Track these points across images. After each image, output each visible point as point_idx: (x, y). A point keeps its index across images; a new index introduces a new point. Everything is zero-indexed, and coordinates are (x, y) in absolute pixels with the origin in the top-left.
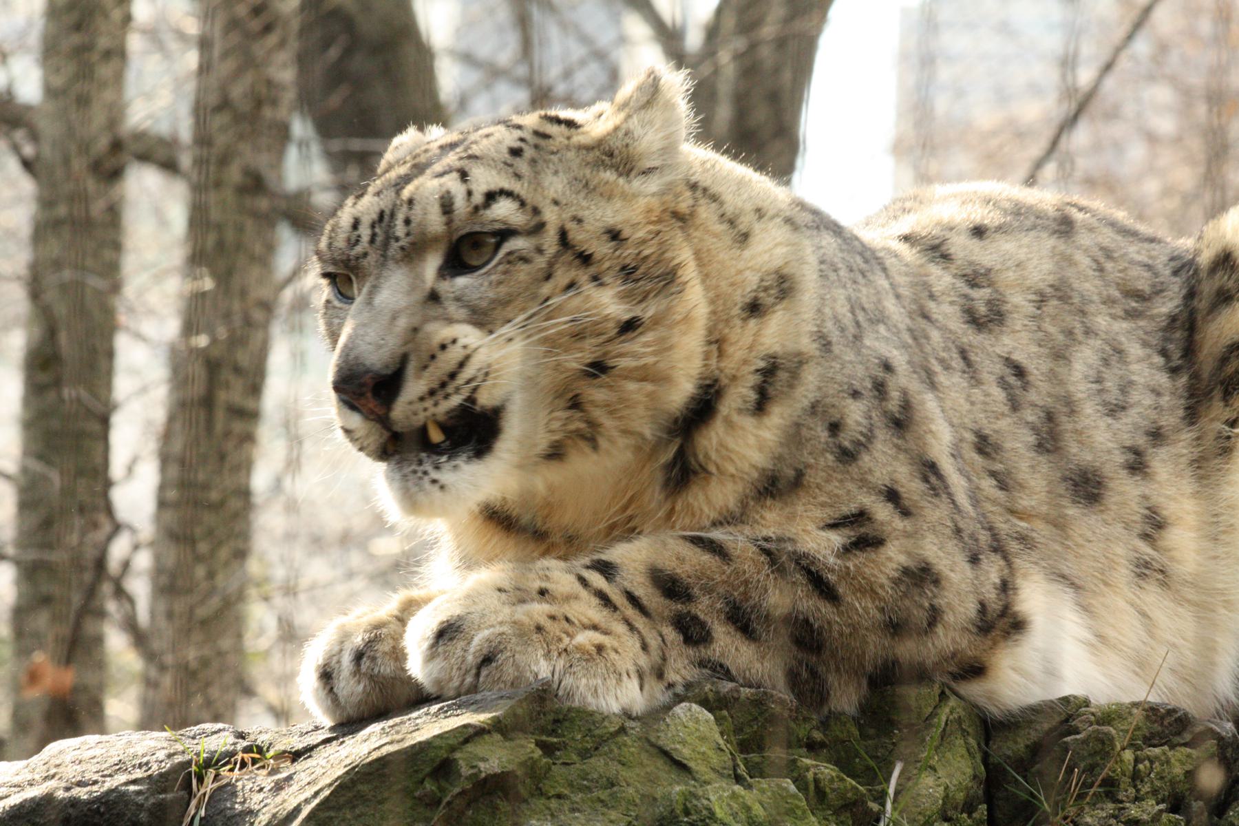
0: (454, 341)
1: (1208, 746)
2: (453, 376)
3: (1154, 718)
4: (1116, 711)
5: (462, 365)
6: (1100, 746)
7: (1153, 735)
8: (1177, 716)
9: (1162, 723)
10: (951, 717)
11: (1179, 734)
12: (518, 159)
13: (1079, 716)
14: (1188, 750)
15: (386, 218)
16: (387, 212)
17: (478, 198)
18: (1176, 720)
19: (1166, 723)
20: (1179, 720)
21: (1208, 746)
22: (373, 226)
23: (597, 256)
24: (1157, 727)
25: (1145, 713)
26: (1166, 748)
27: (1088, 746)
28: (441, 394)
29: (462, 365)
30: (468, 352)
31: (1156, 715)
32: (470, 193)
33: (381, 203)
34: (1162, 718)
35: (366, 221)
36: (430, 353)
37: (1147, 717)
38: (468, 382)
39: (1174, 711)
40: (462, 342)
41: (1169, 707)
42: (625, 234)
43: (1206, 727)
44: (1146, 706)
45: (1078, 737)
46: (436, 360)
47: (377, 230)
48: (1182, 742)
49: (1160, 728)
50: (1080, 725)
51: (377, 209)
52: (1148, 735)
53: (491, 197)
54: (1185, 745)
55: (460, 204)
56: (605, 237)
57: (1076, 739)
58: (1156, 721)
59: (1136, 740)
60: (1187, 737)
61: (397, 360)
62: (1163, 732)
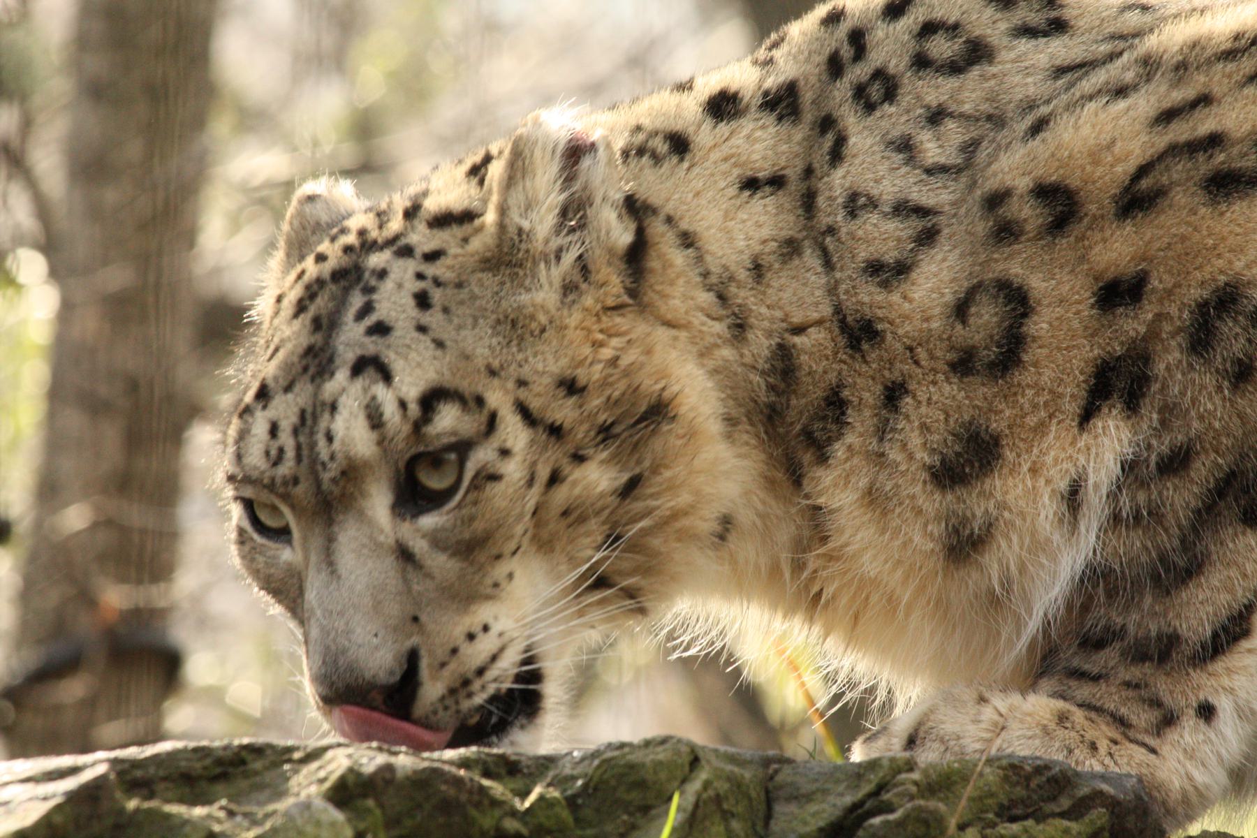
0: (486, 628)
1: (1094, 817)
2: (481, 672)
3: (1015, 778)
4: (959, 772)
5: (494, 658)
6: (923, 829)
7: (1013, 803)
8: (1050, 774)
9: (1028, 786)
10: (705, 796)
11: (1054, 799)
12: (416, 290)
13: (895, 785)
14: (1066, 823)
15: (308, 416)
16: (309, 410)
17: (414, 409)
18: (1048, 781)
19: (1033, 785)
20: (1053, 780)
21: (1094, 817)
22: (296, 432)
23: (567, 426)
24: (1020, 792)
25: (1001, 772)
26: (1030, 823)
27: (905, 830)
28: (463, 693)
29: (494, 658)
30: (506, 638)
31: (1018, 775)
32: (403, 404)
33: (299, 400)
34: (1028, 778)
35: (286, 426)
36: (452, 646)
37: (1006, 778)
38: (495, 680)
39: (1047, 767)
40: (496, 628)
41: (1039, 762)
42: (582, 381)
43: (1094, 789)
44: (1004, 762)
45: (891, 817)
46: (459, 654)
47: (302, 439)
48: (1058, 810)
49: (1024, 792)
50: (895, 800)
51: (296, 410)
52: (1006, 803)
53: (391, 310)
54: (1063, 815)
55: (390, 410)
56: (562, 392)
57: (888, 822)
58: (1018, 783)
59: (987, 811)
60: (1065, 803)
61: (404, 660)
62: (1029, 797)
